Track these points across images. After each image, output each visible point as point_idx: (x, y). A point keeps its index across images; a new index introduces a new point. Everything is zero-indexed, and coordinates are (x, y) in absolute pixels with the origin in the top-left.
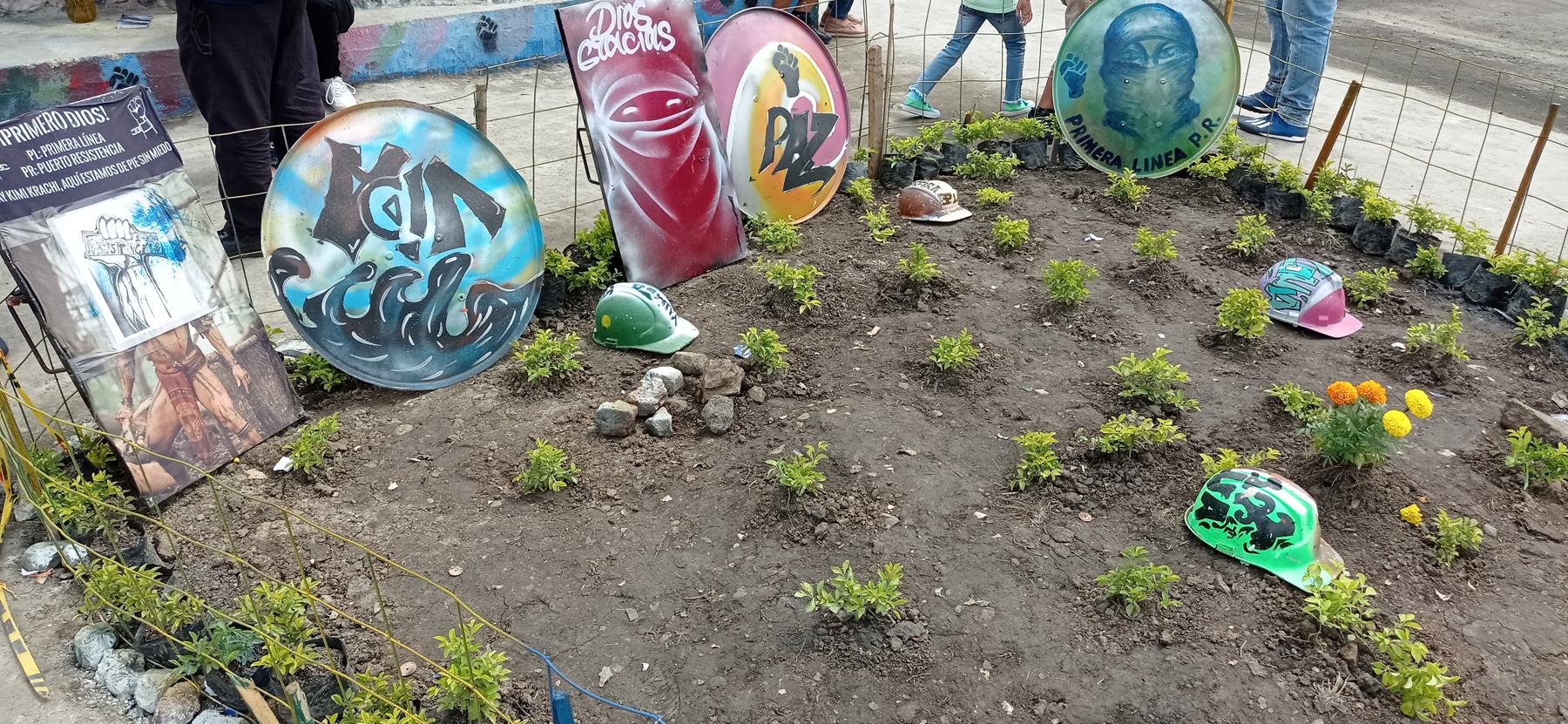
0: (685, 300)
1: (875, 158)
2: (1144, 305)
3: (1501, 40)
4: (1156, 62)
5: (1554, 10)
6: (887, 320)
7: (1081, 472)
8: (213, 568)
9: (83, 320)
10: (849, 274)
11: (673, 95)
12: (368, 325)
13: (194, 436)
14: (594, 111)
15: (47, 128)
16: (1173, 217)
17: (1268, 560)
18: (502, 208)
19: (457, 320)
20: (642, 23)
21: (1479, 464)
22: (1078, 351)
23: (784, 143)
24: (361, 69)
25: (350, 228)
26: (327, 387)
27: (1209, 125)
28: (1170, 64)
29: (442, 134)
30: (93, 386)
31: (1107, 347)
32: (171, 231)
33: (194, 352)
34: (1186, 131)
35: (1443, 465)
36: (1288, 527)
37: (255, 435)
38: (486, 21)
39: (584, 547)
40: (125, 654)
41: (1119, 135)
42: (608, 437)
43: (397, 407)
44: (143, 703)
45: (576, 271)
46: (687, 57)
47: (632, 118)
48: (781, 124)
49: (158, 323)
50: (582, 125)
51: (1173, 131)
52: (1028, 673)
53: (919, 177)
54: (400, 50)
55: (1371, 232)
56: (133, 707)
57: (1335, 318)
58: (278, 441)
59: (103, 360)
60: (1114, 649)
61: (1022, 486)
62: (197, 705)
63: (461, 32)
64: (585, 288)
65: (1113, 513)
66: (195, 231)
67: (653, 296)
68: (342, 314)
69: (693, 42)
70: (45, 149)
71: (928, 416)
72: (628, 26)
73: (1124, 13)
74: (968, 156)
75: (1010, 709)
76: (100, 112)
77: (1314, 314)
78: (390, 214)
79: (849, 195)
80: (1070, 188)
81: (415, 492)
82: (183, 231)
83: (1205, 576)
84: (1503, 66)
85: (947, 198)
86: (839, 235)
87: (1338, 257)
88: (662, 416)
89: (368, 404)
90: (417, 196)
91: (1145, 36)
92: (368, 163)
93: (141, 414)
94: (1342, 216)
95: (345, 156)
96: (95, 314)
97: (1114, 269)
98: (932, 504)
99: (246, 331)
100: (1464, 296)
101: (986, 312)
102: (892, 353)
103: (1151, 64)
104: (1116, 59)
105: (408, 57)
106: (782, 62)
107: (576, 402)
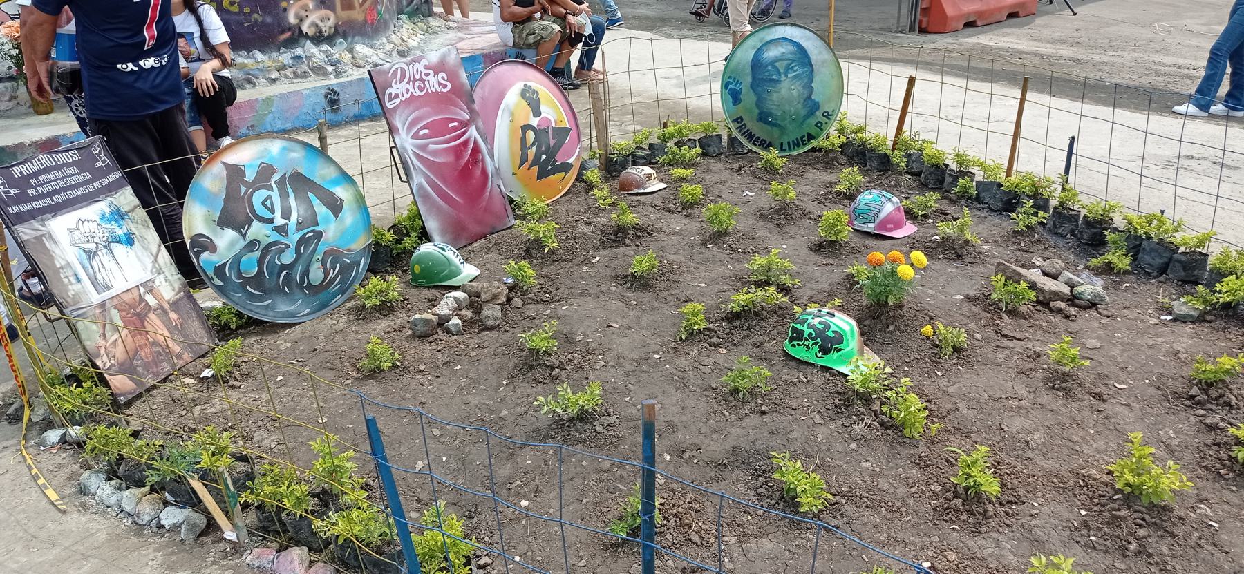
0: (472, 254)
1: (603, 157)
2: (776, 230)
3: (1072, 48)
4: (786, 76)
5: (1112, 24)
6: (606, 252)
7: (722, 327)
8: (166, 434)
9: (71, 284)
10: (582, 228)
11: (453, 120)
12: (257, 280)
13: (147, 358)
14: (399, 134)
15: (42, 165)
16: (805, 177)
17: (830, 360)
18: (341, 200)
19: (316, 274)
20: (427, 75)
21: (978, 301)
22: (727, 259)
23: (534, 148)
24: (244, 130)
25: (241, 218)
26: (233, 327)
27: (827, 115)
28: (796, 77)
29: (297, 154)
30: (80, 326)
31: (747, 256)
32: (124, 227)
33: (144, 303)
34: (813, 121)
35: (955, 304)
36: (839, 338)
37: (187, 357)
38: (331, 91)
39: (405, 400)
40: (113, 483)
41: (769, 128)
42: (420, 337)
43: (280, 334)
44: (127, 508)
45: (397, 241)
46: (462, 95)
47: (425, 137)
48: (531, 136)
49: (119, 286)
50: (393, 145)
51: (803, 122)
52: (679, 436)
53: (634, 164)
54: (271, 115)
55: (931, 174)
56: (121, 512)
57: (898, 226)
58: (203, 360)
59: (85, 309)
60: (733, 418)
61: (683, 337)
62: (162, 506)
63: (313, 100)
64: (404, 253)
65: (741, 348)
66: (140, 226)
67: (446, 249)
68: (239, 275)
69: (463, 85)
70: (42, 178)
71: (627, 304)
72: (418, 77)
73: (761, 47)
74: (666, 150)
75: (668, 457)
76: (75, 154)
77: (883, 224)
78: (266, 207)
79: (585, 182)
80: (736, 166)
81: (294, 380)
82: (132, 227)
83: (792, 374)
84: (1070, 66)
85: (649, 176)
86: (577, 206)
87: (911, 192)
88: (455, 321)
89: (260, 334)
90: (284, 195)
91: (778, 60)
92: (250, 176)
93: (112, 343)
94: (914, 165)
95: (235, 172)
96: (79, 280)
97: (760, 211)
98: (627, 353)
99: (177, 289)
100: (989, 207)
101: (671, 243)
102: (608, 272)
103: (783, 78)
104: (760, 77)
105: (277, 120)
106: (528, 95)
107: (399, 319)
